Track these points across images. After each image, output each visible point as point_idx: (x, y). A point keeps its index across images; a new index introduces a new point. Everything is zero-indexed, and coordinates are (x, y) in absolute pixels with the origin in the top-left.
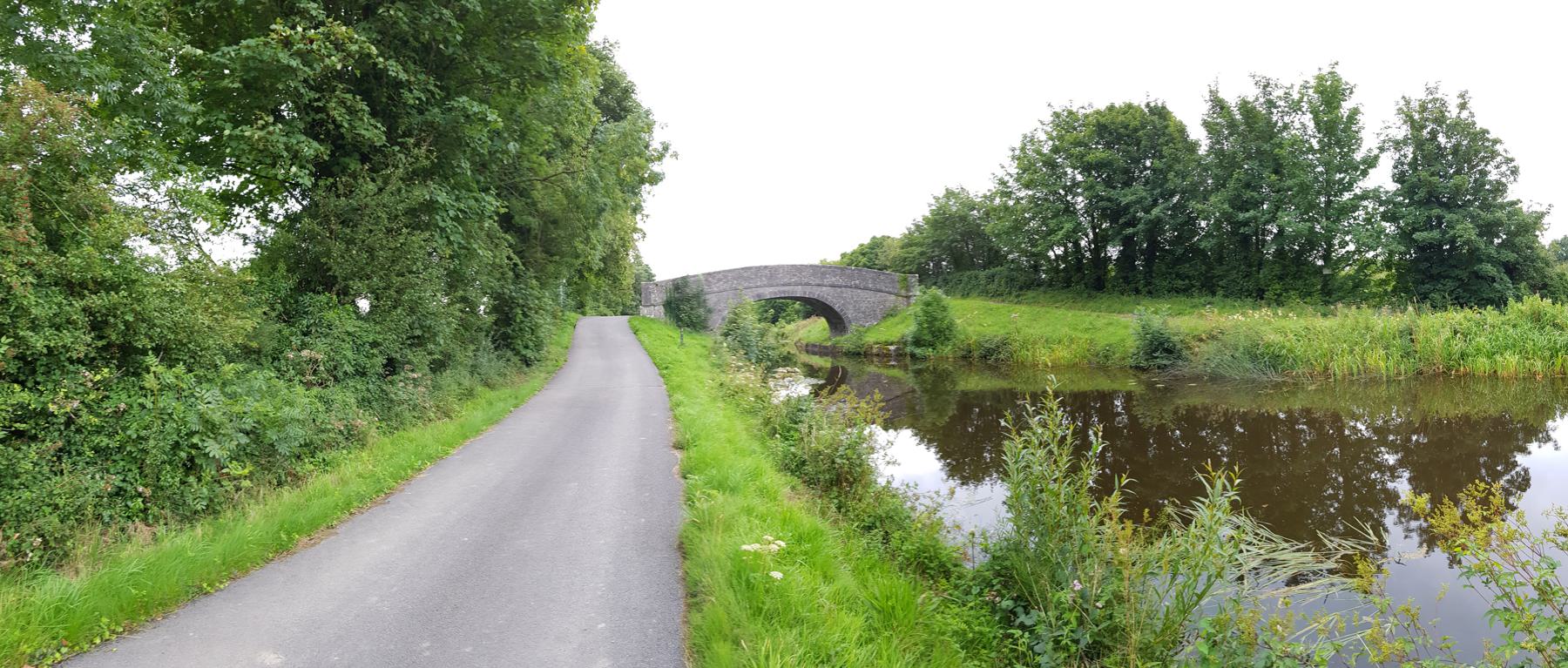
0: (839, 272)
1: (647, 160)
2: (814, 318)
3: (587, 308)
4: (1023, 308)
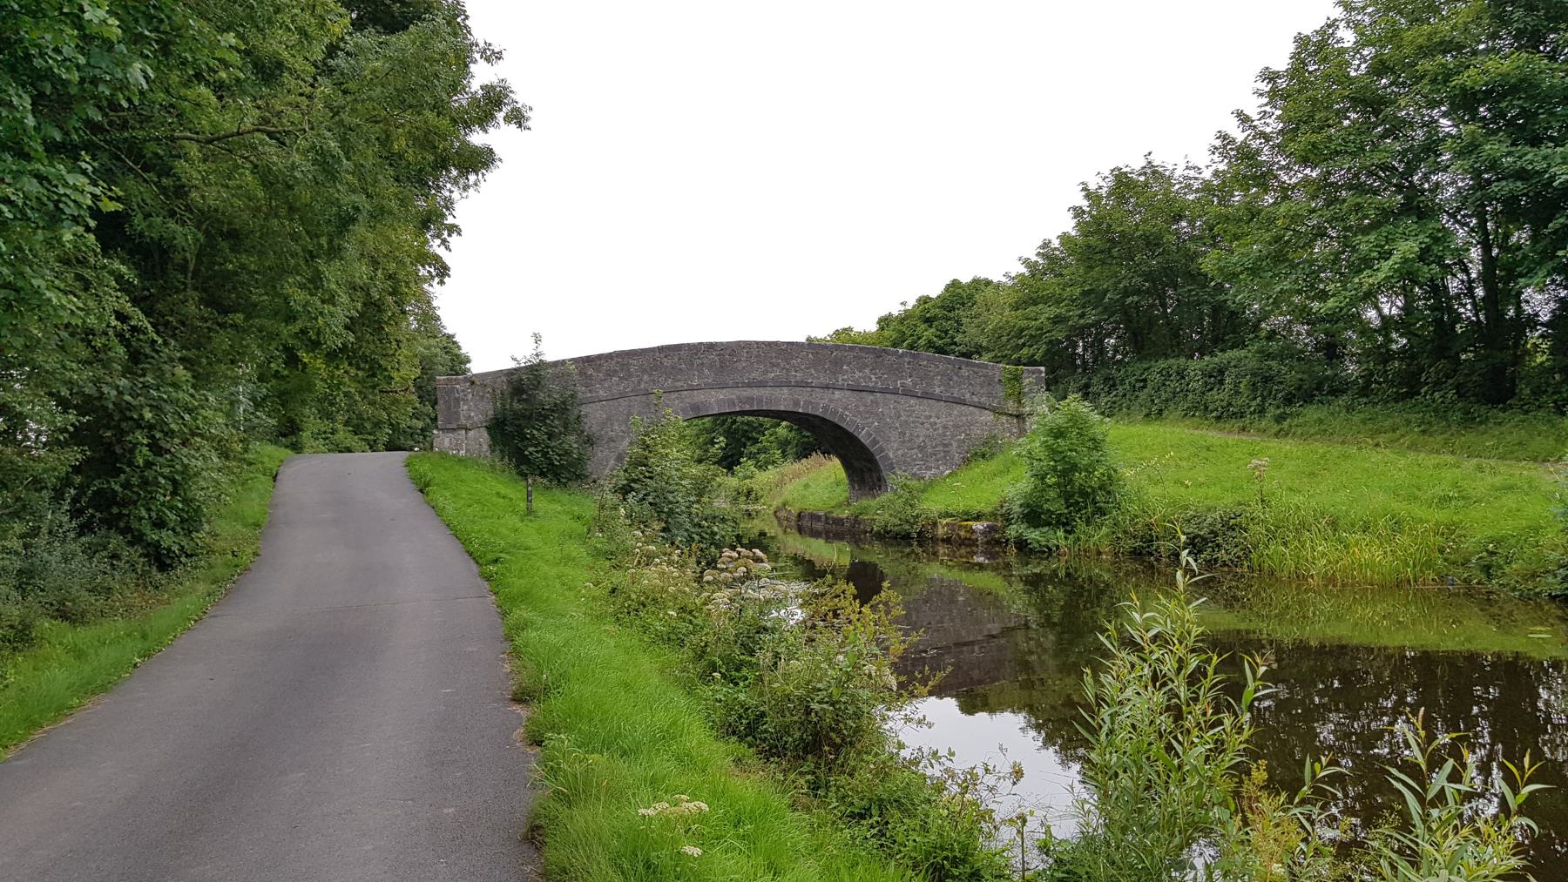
0: (869, 359)
1: (454, 121)
2: (816, 458)
3: (306, 435)
4: (1289, 446)
